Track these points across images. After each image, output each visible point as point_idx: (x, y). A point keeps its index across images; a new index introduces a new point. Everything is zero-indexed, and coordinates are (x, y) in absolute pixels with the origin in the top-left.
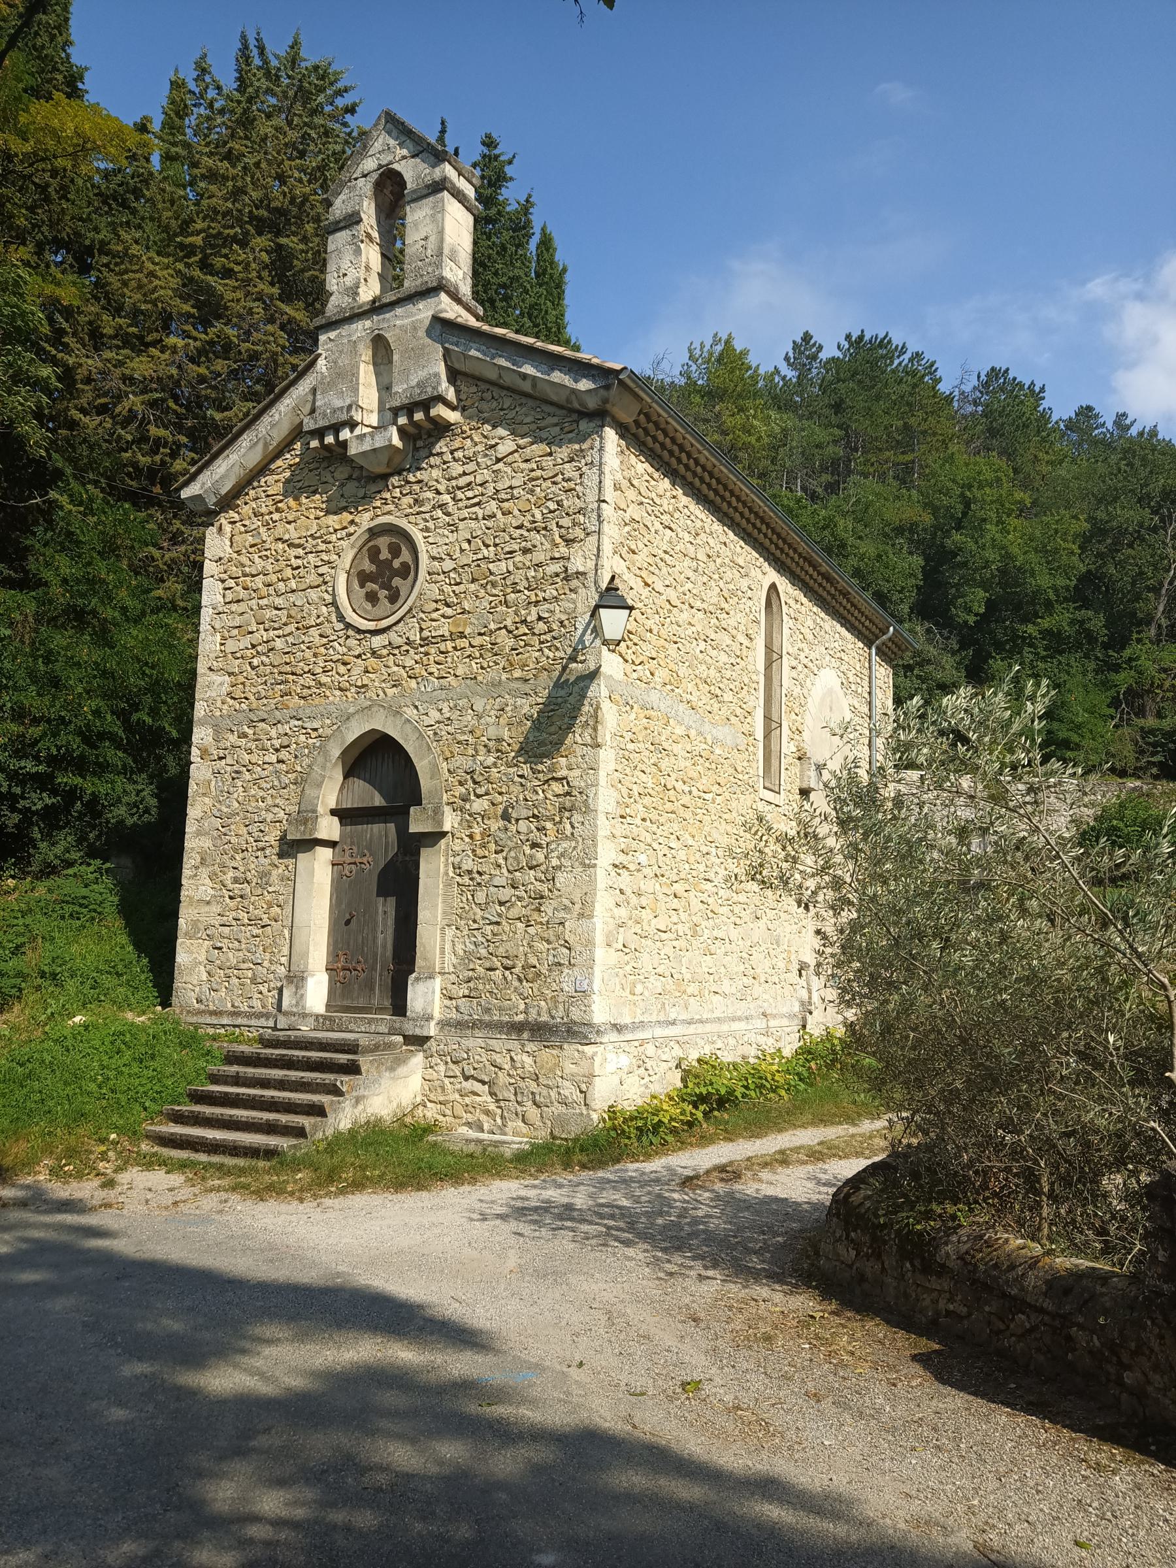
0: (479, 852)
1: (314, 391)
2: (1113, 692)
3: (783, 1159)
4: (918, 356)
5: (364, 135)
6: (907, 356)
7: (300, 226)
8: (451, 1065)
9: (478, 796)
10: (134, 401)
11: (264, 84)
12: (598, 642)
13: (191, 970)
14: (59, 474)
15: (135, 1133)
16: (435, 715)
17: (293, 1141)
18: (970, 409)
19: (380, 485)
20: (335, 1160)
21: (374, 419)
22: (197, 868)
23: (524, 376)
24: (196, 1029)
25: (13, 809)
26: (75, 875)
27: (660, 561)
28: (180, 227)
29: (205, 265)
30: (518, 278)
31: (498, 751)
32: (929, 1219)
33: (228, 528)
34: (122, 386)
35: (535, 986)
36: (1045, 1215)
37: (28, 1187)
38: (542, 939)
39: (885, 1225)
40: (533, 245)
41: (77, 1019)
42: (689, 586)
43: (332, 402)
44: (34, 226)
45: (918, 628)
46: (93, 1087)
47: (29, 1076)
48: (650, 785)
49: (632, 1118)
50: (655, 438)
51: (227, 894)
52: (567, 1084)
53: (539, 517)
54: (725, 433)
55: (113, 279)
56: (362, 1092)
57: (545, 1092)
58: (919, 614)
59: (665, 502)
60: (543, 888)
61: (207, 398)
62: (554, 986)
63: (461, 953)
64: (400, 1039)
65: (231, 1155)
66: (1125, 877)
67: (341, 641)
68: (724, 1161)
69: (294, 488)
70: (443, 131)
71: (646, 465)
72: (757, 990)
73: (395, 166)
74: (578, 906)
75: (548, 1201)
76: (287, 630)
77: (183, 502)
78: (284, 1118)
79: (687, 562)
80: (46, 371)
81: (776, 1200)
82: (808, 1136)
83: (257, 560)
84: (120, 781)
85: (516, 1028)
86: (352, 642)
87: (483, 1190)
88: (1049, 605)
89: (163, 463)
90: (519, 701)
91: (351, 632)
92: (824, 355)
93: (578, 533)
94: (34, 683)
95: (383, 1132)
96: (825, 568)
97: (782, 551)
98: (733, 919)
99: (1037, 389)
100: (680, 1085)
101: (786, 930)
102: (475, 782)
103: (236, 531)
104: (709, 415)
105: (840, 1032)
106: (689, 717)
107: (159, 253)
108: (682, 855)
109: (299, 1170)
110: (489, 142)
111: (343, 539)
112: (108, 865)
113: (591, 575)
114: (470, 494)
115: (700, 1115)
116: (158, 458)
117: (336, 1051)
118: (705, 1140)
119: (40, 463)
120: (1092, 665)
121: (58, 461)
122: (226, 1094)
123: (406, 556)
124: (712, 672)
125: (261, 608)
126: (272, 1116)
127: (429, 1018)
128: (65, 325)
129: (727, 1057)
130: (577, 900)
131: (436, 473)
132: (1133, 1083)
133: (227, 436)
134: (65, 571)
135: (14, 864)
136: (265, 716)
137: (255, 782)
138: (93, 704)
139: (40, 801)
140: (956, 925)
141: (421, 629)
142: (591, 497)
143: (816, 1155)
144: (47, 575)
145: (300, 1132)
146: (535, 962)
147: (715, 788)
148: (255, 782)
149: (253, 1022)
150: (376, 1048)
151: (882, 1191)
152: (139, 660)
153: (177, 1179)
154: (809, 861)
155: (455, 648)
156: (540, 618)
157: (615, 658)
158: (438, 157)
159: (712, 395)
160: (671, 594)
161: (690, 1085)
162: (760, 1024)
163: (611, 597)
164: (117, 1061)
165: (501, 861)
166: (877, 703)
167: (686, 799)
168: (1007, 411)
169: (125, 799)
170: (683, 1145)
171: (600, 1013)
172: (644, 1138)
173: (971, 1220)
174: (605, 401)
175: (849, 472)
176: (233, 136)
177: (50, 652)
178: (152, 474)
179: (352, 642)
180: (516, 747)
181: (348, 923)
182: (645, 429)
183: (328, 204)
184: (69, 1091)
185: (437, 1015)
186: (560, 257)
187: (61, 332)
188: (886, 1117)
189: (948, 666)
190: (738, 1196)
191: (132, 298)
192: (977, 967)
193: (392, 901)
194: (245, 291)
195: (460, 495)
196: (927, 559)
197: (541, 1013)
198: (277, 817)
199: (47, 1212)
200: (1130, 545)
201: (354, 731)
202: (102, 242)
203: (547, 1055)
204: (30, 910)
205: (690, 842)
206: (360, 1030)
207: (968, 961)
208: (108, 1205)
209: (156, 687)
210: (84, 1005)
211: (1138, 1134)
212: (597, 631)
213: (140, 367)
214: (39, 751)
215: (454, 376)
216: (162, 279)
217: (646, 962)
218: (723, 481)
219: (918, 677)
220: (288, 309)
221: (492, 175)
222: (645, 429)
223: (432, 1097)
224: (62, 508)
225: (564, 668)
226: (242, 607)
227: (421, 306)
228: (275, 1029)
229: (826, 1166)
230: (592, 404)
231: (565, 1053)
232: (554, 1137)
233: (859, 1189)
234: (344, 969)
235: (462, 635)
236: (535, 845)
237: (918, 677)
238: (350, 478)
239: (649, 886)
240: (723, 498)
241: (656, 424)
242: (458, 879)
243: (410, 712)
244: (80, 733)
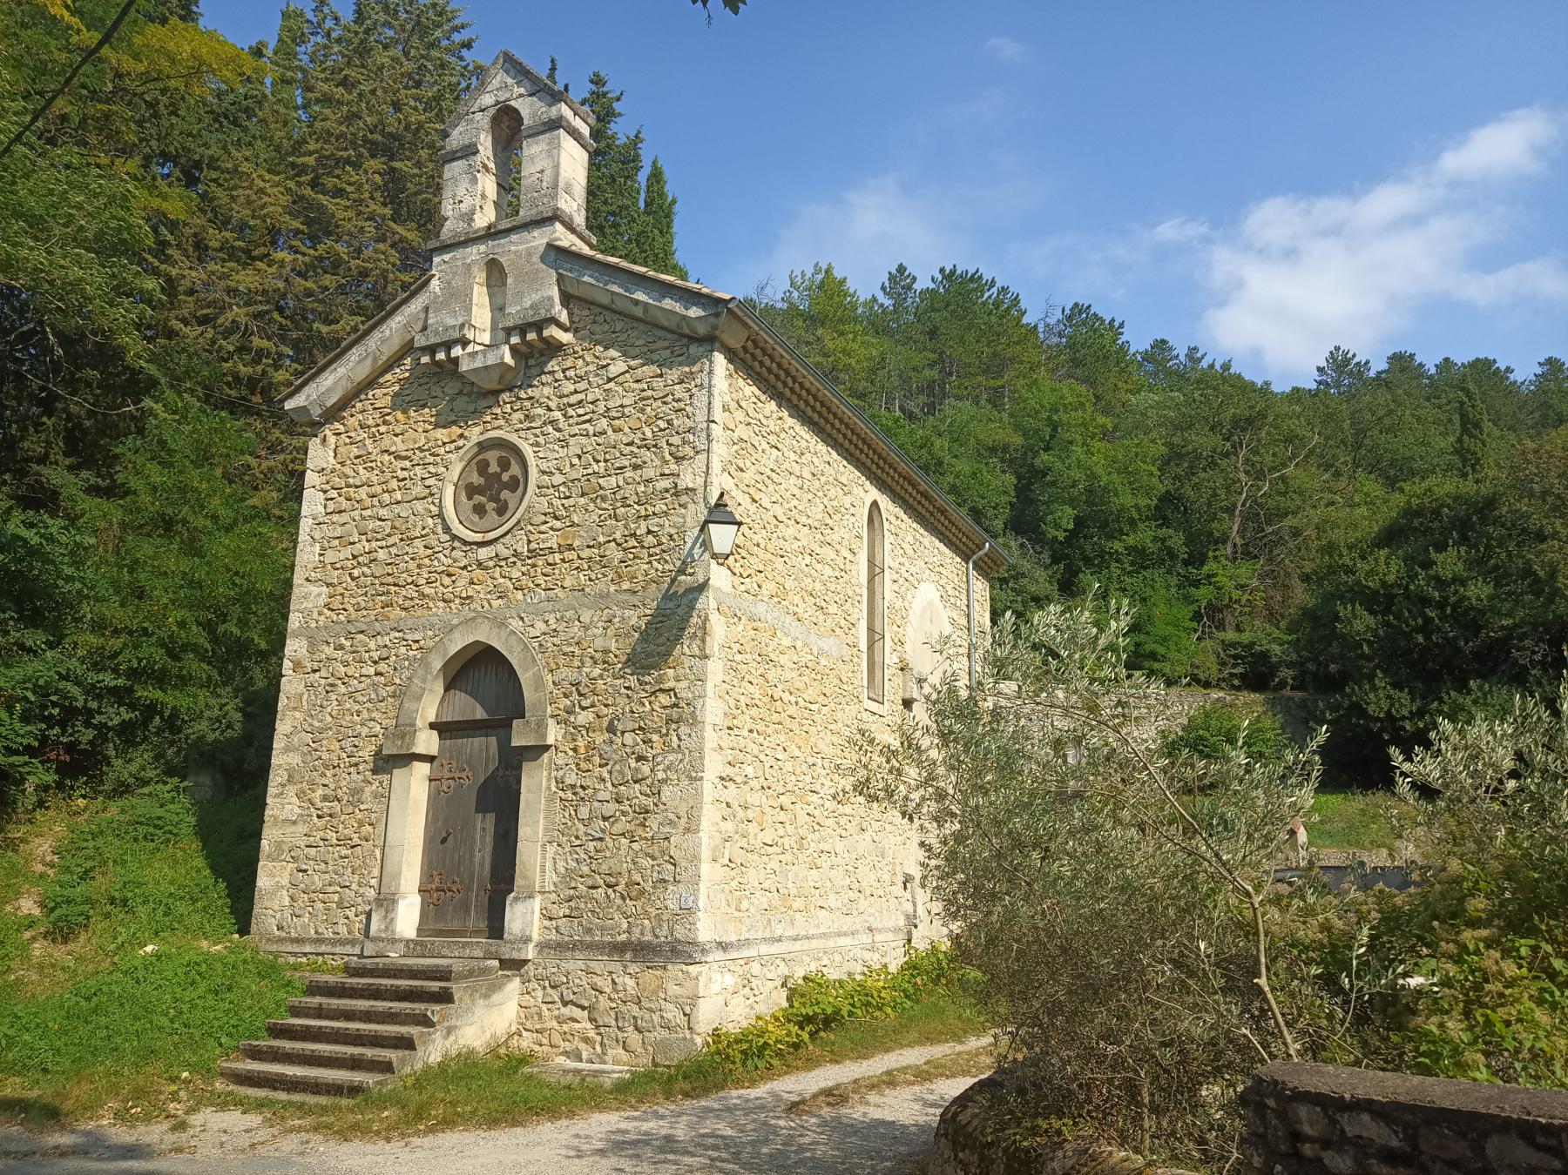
0: (583, 765)
1: (426, 309)
2: (1195, 607)
3: (889, 1080)
4: (1004, 290)
5: (480, 72)
6: (994, 290)
7: (414, 151)
8: (549, 990)
9: (583, 709)
10: (238, 313)
11: (382, 17)
12: (707, 556)
14: (153, 382)
15: (209, 1071)
17: (379, 1077)
18: (1055, 340)
19: (491, 400)
20: (424, 1097)
21: (486, 338)
22: (283, 786)
23: (636, 302)
24: (276, 958)
25: (87, 724)
26: (150, 794)
27: (768, 478)
28: (293, 147)
29: (314, 184)
30: (627, 208)
31: (605, 662)
32: (1035, 1135)
33: (332, 440)
34: (226, 298)
35: (639, 904)
36: (1146, 1126)
37: (89, 1133)
38: (647, 855)
39: (992, 1144)
40: (642, 177)
41: (149, 949)
42: (795, 502)
43: (445, 321)
44: (141, 140)
45: (1012, 543)
46: (164, 1021)
47: (95, 1011)
48: (757, 696)
49: (737, 1041)
50: (761, 363)
51: (314, 813)
52: (670, 1006)
53: (649, 434)
54: (826, 355)
55: (219, 192)
56: (453, 1022)
57: (647, 1016)
58: (1013, 529)
59: (771, 423)
60: (649, 802)
61: (313, 311)
63: (562, 870)
64: (496, 963)
65: (314, 1093)
66: (1212, 786)
67: (447, 552)
68: (830, 1084)
69: (403, 402)
70: (553, 69)
71: (754, 389)
72: (863, 904)
73: (513, 103)
74: (684, 820)
75: (646, 1133)
76: (391, 541)
77: (286, 413)
78: (369, 1053)
79: (793, 480)
80: (150, 284)
81: (883, 1123)
82: (914, 1056)
83: (362, 471)
84: (202, 694)
85: (619, 949)
86: (458, 554)
87: (581, 1124)
88: (1132, 522)
89: (264, 372)
91: (456, 544)
92: (918, 286)
93: (688, 450)
94: (117, 592)
95: (475, 1065)
96: (923, 487)
97: (883, 470)
98: (839, 831)
99: (1116, 324)
100: (785, 1004)
101: (891, 841)
102: (580, 695)
103: (341, 442)
104: (811, 338)
105: (946, 945)
106: (796, 629)
107: (269, 171)
108: (788, 766)
109: (385, 1108)
110: (597, 81)
111: (450, 455)
112: (186, 783)
113: (701, 490)
114: (581, 411)
115: (806, 1036)
116: (259, 368)
117: (428, 978)
118: (812, 1063)
119: (135, 373)
120: (1174, 581)
121: (152, 369)
122: (308, 1027)
123: (515, 469)
124: (818, 585)
125: (364, 518)
126: (357, 1050)
127: (527, 940)
128: (169, 237)
129: (833, 974)
131: (547, 391)
132: (1225, 991)
133: (336, 349)
134: (157, 479)
135: (86, 783)
136: (364, 627)
137: (351, 695)
138: (180, 614)
139: (116, 715)
140: (1053, 836)
141: (529, 542)
142: (701, 417)
143: (923, 1075)
144: (135, 483)
145: (387, 1067)
146: (639, 879)
147: (821, 699)
148: (351, 695)
149: (338, 950)
150: (471, 973)
151: (990, 1107)
152: (229, 570)
153: (254, 1119)
154: (912, 772)
155: (563, 560)
156: (649, 532)
157: (724, 570)
158: (556, 97)
159: (813, 319)
160: (778, 511)
161: (796, 1004)
162: (866, 939)
163: (720, 512)
164: (190, 993)
165: (606, 775)
166: (976, 616)
167: (792, 710)
168: (1088, 344)
169: (207, 714)
170: (790, 1069)
171: (705, 931)
172: (749, 1063)
173: (1074, 1133)
174: (715, 328)
175: (944, 395)
176: (348, 63)
177: (136, 561)
178: (252, 384)
179: (458, 554)
180: (623, 659)
181: (444, 841)
182: (752, 355)
183: (445, 135)
184: (138, 1025)
185: (536, 937)
186: (670, 190)
187: (164, 244)
188: (992, 1032)
189: (1041, 579)
190: (845, 1121)
191: (240, 212)
192: (1075, 877)
193: (491, 817)
194: (356, 206)
195: (571, 412)
196: (1019, 478)
197: (644, 932)
198: (373, 729)
199: (109, 1159)
200: (1204, 470)
201: (457, 643)
202: (211, 158)
203: (650, 976)
204: (102, 832)
205: (797, 753)
206: (451, 956)
207: (1067, 871)
208: (179, 1150)
209: (246, 598)
210: (156, 933)
211: (1231, 1041)
212: (706, 545)
213: (246, 279)
214: (118, 664)
215: (567, 299)
216: (274, 197)
217: (752, 877)
218: (828, 403)
219: (1013, 590)
220: (399, 229)
221: (602, 109)
222: (752, 355)
223: (529, 1026)
224: (156, 417)
225: (673, 581)
226: (344, 518)
227: (536, 234)
228: (361, 956)
229: (933, 1087)
230: (702, 330)
231: (669, 974)
232: (656, 1065)
233: (966, 1107)
234: (438, 890)
235: (570, 548)
236: (640, 758)
237: (1013, 590)
238: (460, 393)
239: (755, 798)
240: (827, 421)
241: (764, 351)
242: (561, 794)
244: (163, 645)
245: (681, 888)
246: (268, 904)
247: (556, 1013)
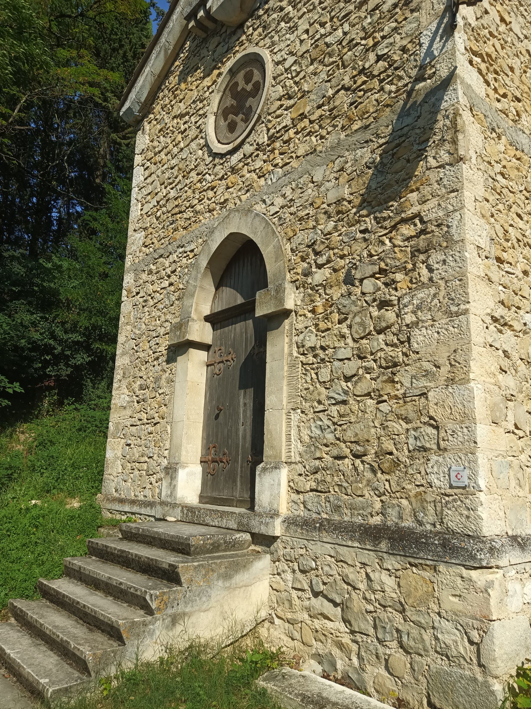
8: (299, 575)
9: (320, 267)
16: (279, 201)
31: (339, 212)
35: (393, 478)
38: (399, 417)
51: (135, 399)
57: (415, 632)
60: (398, 354)
62: (419, 479)
63: (307, 439)
74: (445, 370)
85: (371, 535)
90: (359, 152)
127: (274, 514)
130: (443, 360)
150: (216, 547)
165: (346, 331)
171: (492, 519)
180: (357, 201)
181: (217, 417)
185: (284, 509)
203: (415, 577)
225: (409, 94)
234: (213, 461)
236: (384, 304)
242: (302, 358)
243: (260, 208)
245: (449, 458)
247: (307, 603)
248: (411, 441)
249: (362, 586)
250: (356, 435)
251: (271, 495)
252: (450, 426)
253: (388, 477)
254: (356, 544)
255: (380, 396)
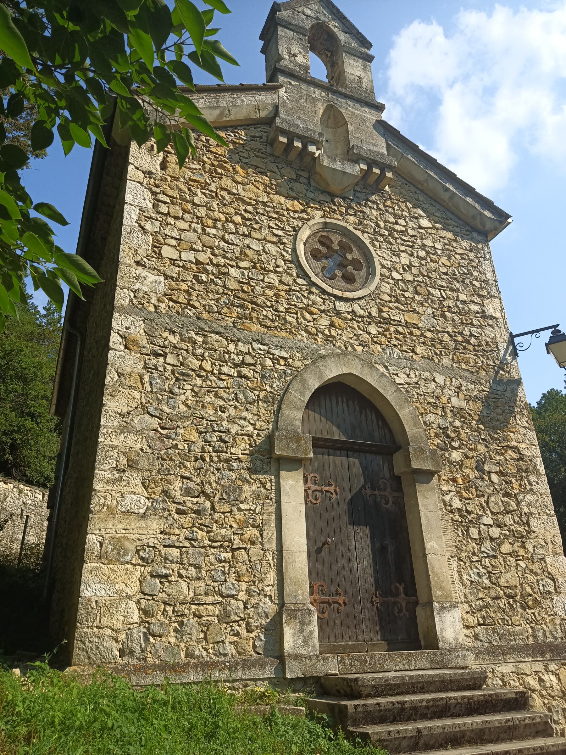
13: (109, 609)
23: (447, 190)
181: (319, 550)
201: (332, 370)
246: (105, 621)
248: (541, 588)
249: (538, 687)
250: (508, 582)
251: (454, 631)
252: (560, 579)
253: (532, 611)
254: (531, 659)
255: (518, 556)
